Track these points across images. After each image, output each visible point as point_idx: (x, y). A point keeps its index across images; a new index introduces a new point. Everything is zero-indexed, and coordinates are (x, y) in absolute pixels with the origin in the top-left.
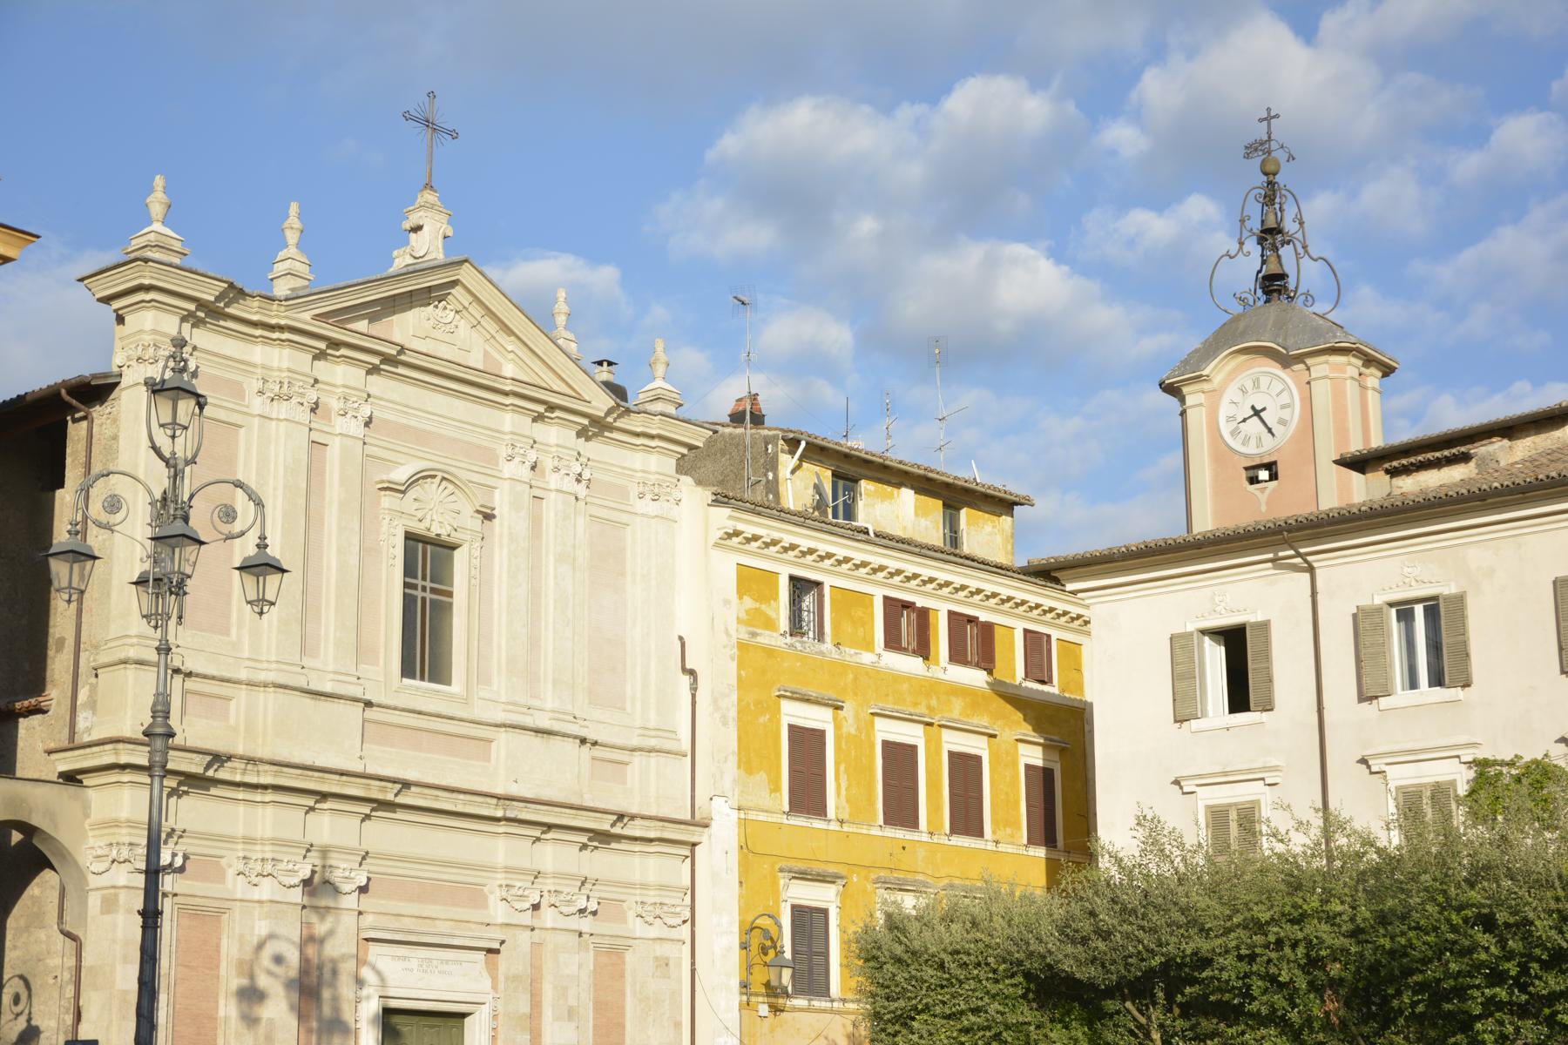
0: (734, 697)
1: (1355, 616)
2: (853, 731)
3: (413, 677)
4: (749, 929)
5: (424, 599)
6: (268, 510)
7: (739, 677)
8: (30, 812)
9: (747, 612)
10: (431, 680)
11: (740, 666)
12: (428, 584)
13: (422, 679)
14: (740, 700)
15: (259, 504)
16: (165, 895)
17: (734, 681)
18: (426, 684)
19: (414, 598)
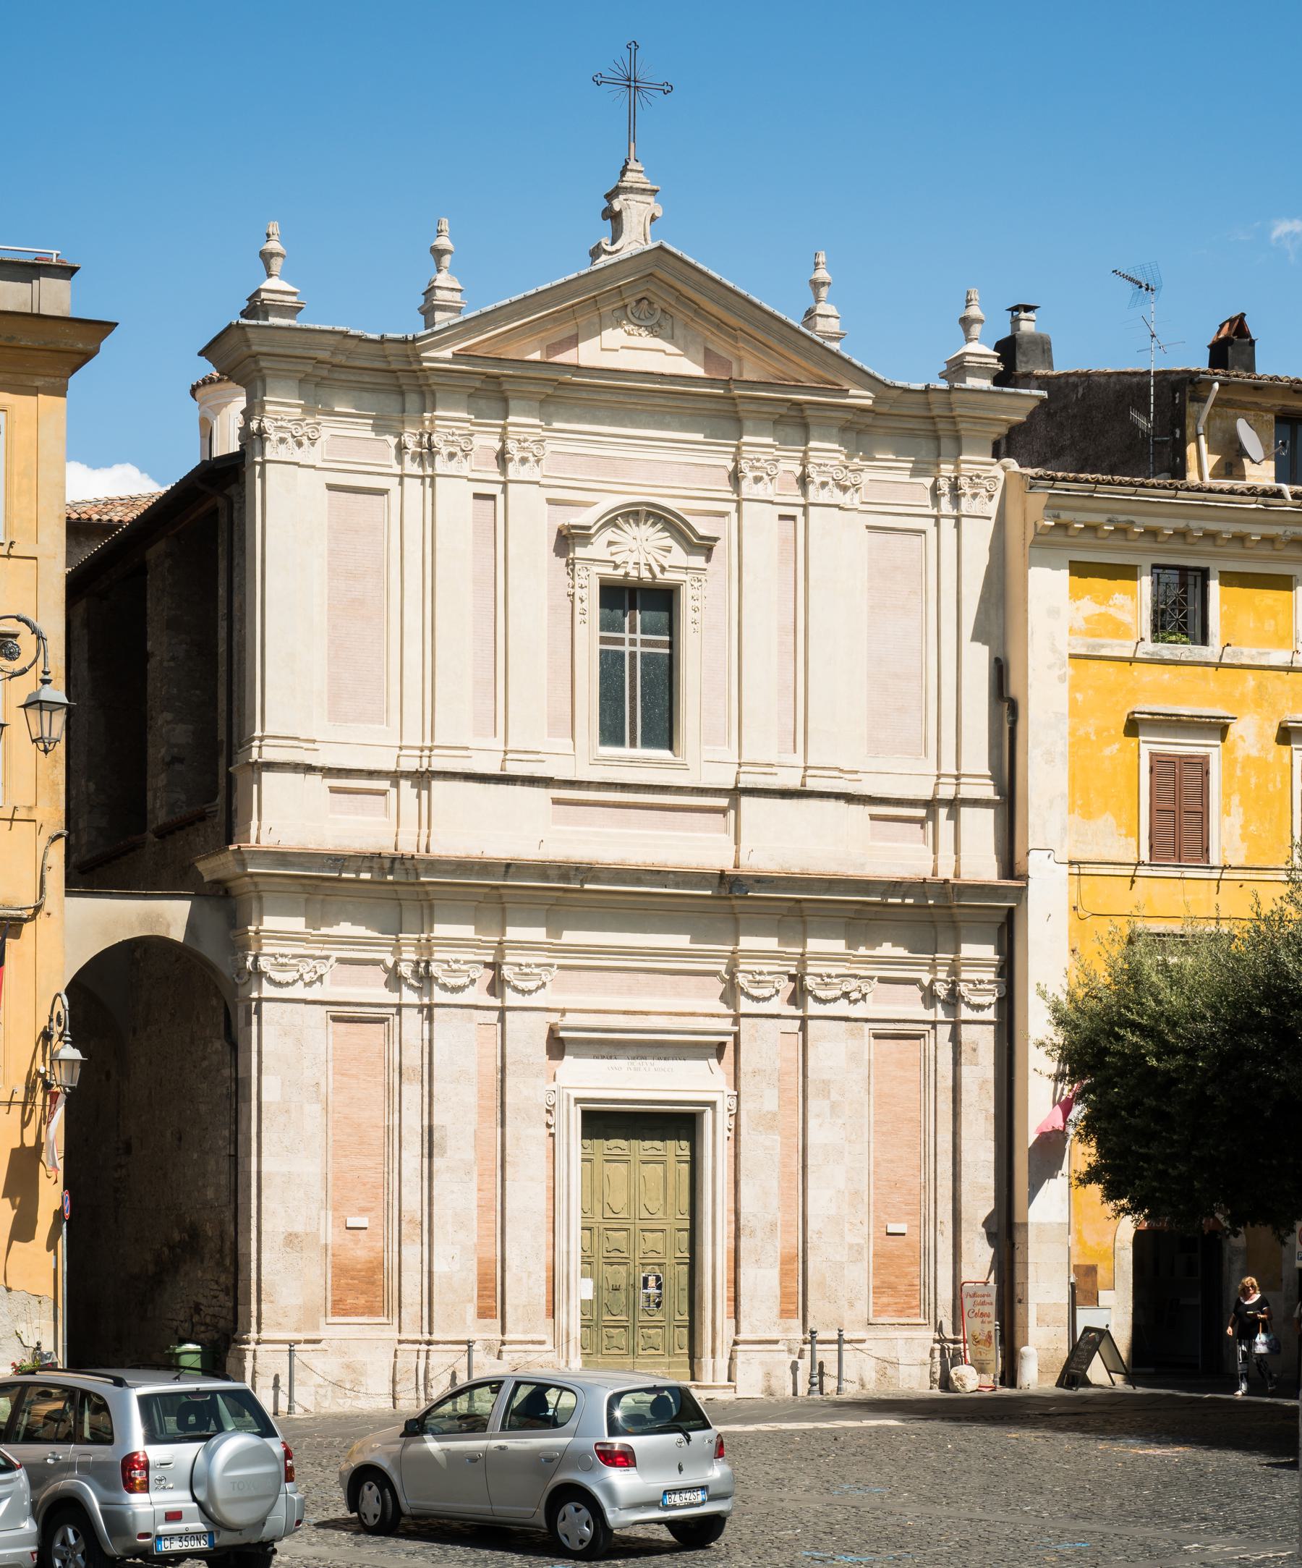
0: (1065, 728)
1: (230, 326)
2: (1254, 752)
3: (619, 741)
4: (883, 1261)
5: (633, 655)
6: (49, 643)
7: (1073, 702)
8: (168, 926)
9: (1087, 620)
10: (648, 743)
11: (1074, 687)
12: (627, 649)
13: (633, 744)
14: (1073, 732)
15: (40, 637)
16: (803, 785)
17: (1065, 709)
18: (640, 752)
19: (621, 655)
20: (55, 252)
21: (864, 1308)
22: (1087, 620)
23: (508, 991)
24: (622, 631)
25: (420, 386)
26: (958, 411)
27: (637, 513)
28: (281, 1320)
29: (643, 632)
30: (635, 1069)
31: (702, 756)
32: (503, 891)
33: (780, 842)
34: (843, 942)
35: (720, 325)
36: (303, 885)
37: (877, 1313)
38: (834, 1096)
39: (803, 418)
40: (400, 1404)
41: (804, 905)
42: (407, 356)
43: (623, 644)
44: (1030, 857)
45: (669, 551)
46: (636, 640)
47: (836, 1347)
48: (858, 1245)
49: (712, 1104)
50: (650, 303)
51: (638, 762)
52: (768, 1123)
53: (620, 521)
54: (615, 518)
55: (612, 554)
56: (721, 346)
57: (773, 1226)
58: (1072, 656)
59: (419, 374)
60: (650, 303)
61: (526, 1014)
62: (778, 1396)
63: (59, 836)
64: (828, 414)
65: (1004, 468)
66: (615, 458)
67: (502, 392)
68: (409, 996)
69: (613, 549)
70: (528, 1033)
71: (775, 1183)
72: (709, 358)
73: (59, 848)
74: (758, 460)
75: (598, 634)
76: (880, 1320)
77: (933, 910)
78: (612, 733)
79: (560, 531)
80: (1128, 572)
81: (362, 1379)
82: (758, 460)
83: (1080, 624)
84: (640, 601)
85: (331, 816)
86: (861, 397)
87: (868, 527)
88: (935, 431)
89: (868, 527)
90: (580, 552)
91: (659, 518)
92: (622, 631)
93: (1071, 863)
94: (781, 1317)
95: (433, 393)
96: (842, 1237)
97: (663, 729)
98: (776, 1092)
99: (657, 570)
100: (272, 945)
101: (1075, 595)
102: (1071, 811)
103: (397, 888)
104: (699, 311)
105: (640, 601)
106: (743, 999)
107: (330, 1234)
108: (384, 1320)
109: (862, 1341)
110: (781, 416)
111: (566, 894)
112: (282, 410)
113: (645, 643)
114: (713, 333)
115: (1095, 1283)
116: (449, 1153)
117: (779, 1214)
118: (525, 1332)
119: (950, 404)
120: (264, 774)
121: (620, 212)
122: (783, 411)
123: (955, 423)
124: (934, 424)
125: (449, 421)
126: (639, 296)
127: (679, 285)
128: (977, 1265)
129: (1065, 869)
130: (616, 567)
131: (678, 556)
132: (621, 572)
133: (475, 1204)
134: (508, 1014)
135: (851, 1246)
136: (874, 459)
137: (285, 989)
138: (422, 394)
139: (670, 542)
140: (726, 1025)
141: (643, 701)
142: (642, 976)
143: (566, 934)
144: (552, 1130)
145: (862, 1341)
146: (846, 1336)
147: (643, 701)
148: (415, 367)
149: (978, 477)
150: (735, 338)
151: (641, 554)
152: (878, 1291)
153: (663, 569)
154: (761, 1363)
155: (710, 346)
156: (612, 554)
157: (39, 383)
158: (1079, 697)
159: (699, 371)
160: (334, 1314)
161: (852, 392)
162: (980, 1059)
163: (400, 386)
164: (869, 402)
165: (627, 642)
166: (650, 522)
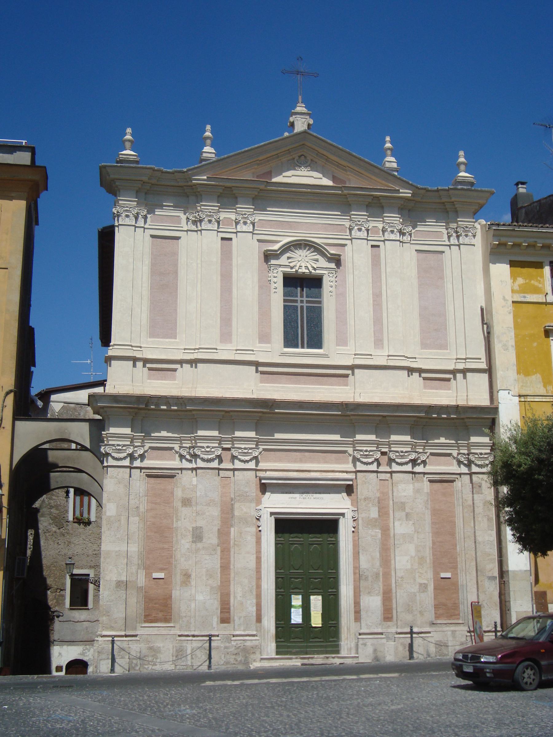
3: (296, 346)
8: (70, 434)
10: (310, 346)
11: (515, 317)
13: (303, 347)
20: (24, 141)
21: (430, 615)
22: (519, 286)
23: (473, 466)
24: (297, 297)
25: (195, 193)
26: (453, 199)
27: (301, 244)
28: (113, 625)
29: (307, 297)
30: (304, 498)
31: (333, 353)
32: (231, 413)
33: (367, 390)
34: (410, 437)
35: (339, 165)
36: (129, 412)
37: (437, 617)
38: (407, 510)
39: (456, 208)
40: (118, 669)
41: (387, 418)
42: (186, 179)
43: (297, 303)
44: (499, 393)
45: (318, 261)
46: (302, 299)
47: (409, 635)
48: (424, 584)
49: (343, 515)
50: (305, 157)
51: (303, 355)
52: (371, 523)
53: (292, 248)
54: (290, 246)
55: (289, 263)
56: (340, 174)
57: (377, 575)
58: (513, 302)
59: (194, 187)
60: (305, 157)
61: (245, 472)
62: (382, 662)
63: (11, 391)
64: (392, 201)
65: (479, 224)
66: (291, 222)
67: (234, 194)
68: (464, 470)
69: (290, 260)
70: (246, 481)
71: (378, 554)
72: (334, 179)
73: (10, 399)
74: (359, 221)
75: (282, 298)
76: (439, 622)
77: (455, 421)
78: (290, 340)
79: (264, 253)
80: (539, 265)
81: (158, 655)
82: (359, 221)
83: (516, 287)
84: (303, 285)
85: (149, 381)
86: (406, 193)
87: (416, 250)
88: (446, 209)
89: (416, 250)
90: (273, 262)
91: (310, 247)
92: (297, 297)
93: (520, 396)
94: (384, 621)
95: (201, 195)
96: (415, 580)
97: (315, 340)
98: (377, 508)
99: (311, 269)
100: (186, 443)
101: (514, 277)
102: (518, 373)
103: (179, 413)
104: (327, 159)
105: (303, 285)
106: (473, 466)
107: (141, 580)
108: (172, 625)
109: (429, 632)
110: (256, 196)
111: (265, 416)
112: (127, 204)
113: (308, 302)
114: (336, 169)
115: (546, 600)
116: (204, 540)
117: (381, 569)
118: (244, 630)
119: (440, 196)
120: (112, 362)
121: (293, 122)
122: (370, 200)
123: (454, 205)
124: (445, 206)
125: (208, 207)
126: (300, 154)
127: (316, 148)
128: (487, 593)
129: (517, 399)
130: (292, 268)
131: (323, 263)
132: (294, 270)
133: (219, 565)
134: (393, 474)
135: (421, 584)
136: (426, 222)
137: (120, 462)
138: (196, 196)
139: (318, 257)
140: (352, 476)
141: (304, 326)
142: (307, 454)
143: (275, 434)
144: (260, 529)
145: (429, 632)
146: (415, 630)
147: (304, 326)
148: (189, 184)
149: (467, 227)
150: (345, 170)
151: (304, 263)
152: (436, 607)
153: (315, 269)
154: (372, 645)
155: (336, 175)
156: (289, 263)
157: (13, 194)
158: (519, 320)
159: (330, 183)
160: (145, 622)
161: (401, 190)
162: (483, 491)
163: (456, 208)
164: (410, 195)
165: (299, 301)
166: (307, 249)
